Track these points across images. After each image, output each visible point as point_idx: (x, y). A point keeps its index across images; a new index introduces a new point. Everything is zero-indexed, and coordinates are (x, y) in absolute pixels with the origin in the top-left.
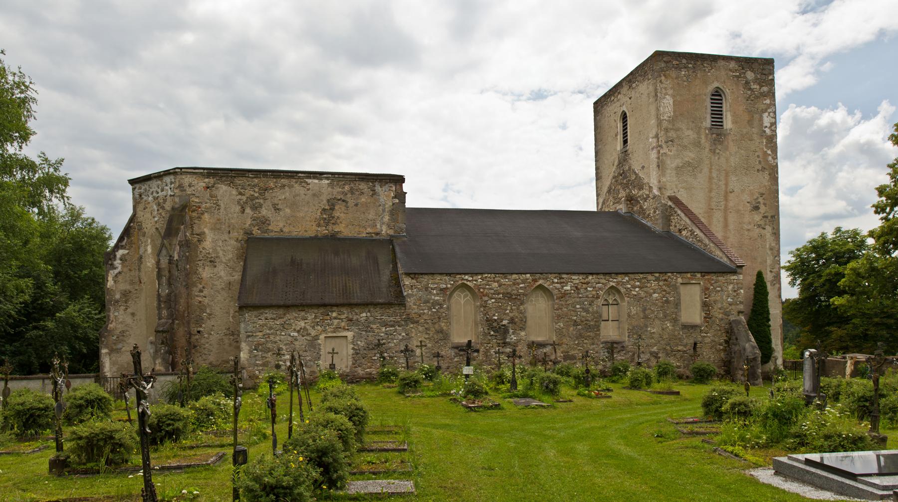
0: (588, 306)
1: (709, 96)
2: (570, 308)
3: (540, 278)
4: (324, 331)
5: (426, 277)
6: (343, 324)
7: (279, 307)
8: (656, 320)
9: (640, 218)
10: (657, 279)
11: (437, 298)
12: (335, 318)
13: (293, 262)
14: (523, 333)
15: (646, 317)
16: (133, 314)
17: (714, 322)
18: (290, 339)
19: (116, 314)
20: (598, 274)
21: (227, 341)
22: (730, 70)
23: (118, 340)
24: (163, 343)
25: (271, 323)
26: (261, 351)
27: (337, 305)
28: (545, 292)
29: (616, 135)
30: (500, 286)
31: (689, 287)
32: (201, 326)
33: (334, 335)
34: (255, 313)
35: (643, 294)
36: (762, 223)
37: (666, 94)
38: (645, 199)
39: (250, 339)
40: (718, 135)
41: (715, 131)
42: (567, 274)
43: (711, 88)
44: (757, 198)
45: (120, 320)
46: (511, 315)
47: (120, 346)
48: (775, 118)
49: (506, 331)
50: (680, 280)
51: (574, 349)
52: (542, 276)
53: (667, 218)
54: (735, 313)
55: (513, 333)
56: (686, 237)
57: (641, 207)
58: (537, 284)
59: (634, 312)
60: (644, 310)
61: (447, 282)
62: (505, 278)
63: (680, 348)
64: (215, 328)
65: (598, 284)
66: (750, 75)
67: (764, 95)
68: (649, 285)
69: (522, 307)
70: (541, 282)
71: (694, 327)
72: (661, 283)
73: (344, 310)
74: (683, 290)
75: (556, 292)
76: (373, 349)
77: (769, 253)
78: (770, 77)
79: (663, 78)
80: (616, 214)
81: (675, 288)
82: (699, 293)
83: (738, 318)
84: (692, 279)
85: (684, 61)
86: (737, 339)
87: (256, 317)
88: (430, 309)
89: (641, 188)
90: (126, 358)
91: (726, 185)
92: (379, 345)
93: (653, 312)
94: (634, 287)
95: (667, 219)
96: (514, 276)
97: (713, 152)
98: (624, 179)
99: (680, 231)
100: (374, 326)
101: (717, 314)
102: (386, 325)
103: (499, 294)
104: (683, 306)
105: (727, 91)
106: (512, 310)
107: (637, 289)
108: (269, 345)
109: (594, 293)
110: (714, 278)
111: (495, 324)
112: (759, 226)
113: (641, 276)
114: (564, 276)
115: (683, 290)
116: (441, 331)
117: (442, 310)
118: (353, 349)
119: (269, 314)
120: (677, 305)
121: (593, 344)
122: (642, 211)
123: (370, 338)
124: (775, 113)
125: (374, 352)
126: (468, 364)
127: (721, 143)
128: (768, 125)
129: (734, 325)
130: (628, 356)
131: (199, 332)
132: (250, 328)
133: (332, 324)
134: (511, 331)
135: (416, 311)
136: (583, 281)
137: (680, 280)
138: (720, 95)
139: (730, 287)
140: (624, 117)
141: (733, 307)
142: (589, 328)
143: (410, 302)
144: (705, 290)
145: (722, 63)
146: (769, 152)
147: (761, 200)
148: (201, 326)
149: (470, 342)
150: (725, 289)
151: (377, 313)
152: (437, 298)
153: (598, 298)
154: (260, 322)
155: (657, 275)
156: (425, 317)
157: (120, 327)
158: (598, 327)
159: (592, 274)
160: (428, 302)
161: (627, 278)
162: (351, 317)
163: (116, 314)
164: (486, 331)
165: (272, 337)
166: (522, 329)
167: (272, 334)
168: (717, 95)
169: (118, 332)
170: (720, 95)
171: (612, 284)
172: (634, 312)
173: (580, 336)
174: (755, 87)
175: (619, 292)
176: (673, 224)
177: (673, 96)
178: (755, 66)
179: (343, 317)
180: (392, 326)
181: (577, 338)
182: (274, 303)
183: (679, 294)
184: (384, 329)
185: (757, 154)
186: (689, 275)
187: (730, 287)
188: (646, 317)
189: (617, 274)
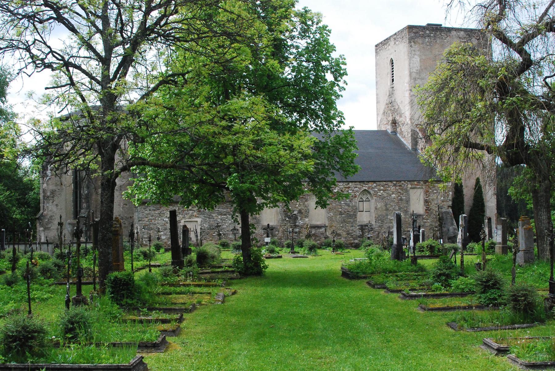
0: (348, 202)
4: (184, 218)
6: (195, 214)
9: (400, 137)
10: (395, 185)
12: (191, 210)
14: (307, 220)
15: (387, 209)
16: (57, 205)
17: (432, 213)
18: (164, 222)
19: (48, 205)
20: (355, 182)
23: (49, 222)
25: (153, 212)
31: (416, 190)
33: (190, 220)
35: (385, 195)
39: (140, 222)
45: (50, 209)
46: (299, 208)
49: (296, 218)
50: (410, 186)
51: (340, 230)
54: (446, 207)
55: (301, 219)
59: (379, 206)
60: (386, 205)
68: (389, 189)
69: (306, 203)
72: (397, 188)
74: (412, 192)
76: (213, 229)
79: (413, 44)
80: (385, 132)
81: (407, 191)
82: (422, 194)
83: (447, 210)
84: (418, 185)
85: (428, 32)
87: (144, 209)
92: (218, 226)
93: (392, 206)
94: (380, 190)
101: (434, 207)
102: (221, 214)
106: (300, 205)
107: (382, 192)
108: (152, 226)
109: (353, 194)
115: (412, 192)
120: (408, 201)
121: (352, 226)
123: (211, 222)
125: (214, 231)
126: (268, 237)
129: (444, 215)
130: (375, 234)
132: (141, 216)
133: (189, 214)
134: (299, 218)
136: (346, 186)
140: (392, 61)
141: (445, 203)
142: (350, 216)
144: (426, 192)
149: (268, 225)
154: (146, 212)
155: (395, 182)
157: (50, 214)
158: (355, 216)
159: (352, 182)
161: (375, 185)
163: (48, 205)
165: (153, 221)
166: (306, 217)
167: (153, 219)
169: (48, 217)
171: (364, 188)
172: (379, 206)
173: (344, 221)
175: (369, 193)
177: (420, 56)
180: (225, 215)
181: (342, 223)
183: (409, 195)
184: (220, 217)
186: (416, 183)
188: (387, 209)
189: (368, 182)
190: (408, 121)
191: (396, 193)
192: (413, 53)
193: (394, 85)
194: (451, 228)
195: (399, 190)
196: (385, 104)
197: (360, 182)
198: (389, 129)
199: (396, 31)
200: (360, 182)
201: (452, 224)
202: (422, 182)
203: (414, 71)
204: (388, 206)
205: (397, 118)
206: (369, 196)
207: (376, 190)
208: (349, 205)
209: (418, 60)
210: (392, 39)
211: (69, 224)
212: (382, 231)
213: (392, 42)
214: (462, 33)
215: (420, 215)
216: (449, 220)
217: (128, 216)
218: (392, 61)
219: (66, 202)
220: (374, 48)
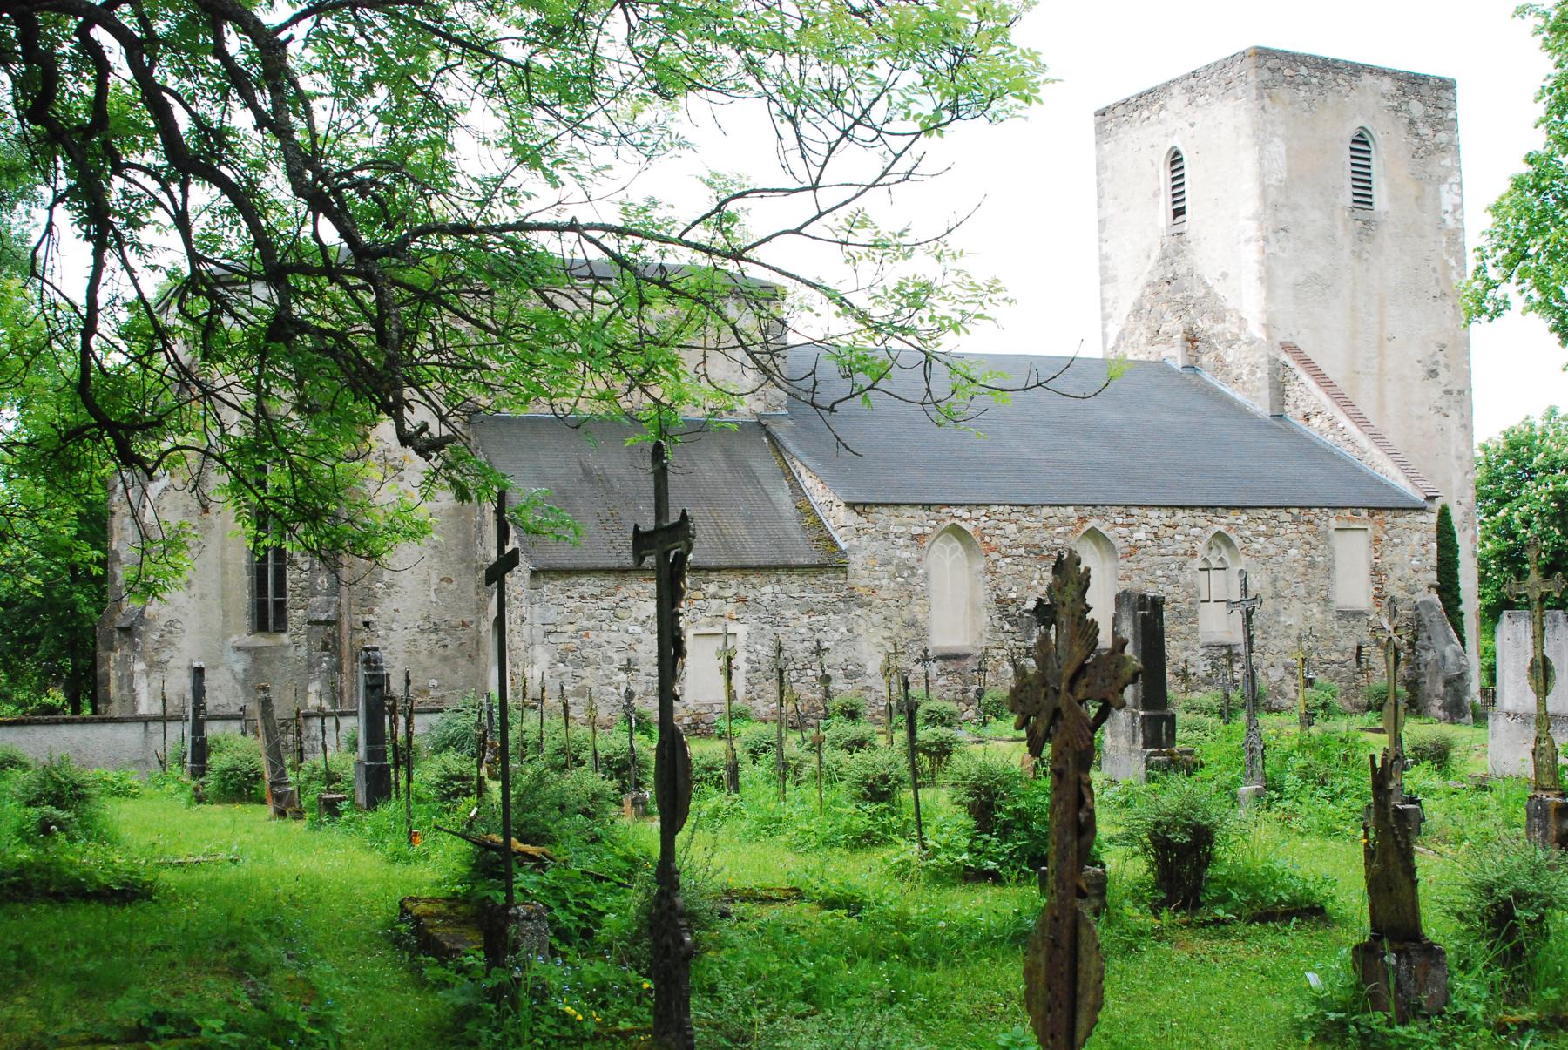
1: (1349, 144)
2: (1145, 576)
3: (1091, 515)
5: (885, 510)
7: (608, 571)
8: (1294, 600)
9: (1215, 382)
10: (1296, 520)
11: (906, 555)
12: (714, 597)
13: (588, 474)
18: (627, 638)
20: (1192, 507)
21: (423, 645)
22: (1383, 96)
24: (325, 647)
25: (591, 605)
26: (572, 663)
27: (718, 569)
28: (1097, 543)
29: (1156, 195)
30: (1020, 531)
32: (371, 612)
34: (560, 584)
35: (1272, 550)
36: (1442, 403)
37: (1273, 134)
38: (1230, 345)
39: (552, 639)
40: (1365, 222)
41: (1360, 214)
42: (1140, 506)
43: (1350, 131)
44: (1434, 354)
47: (164, 656)
48: (1460, 195)
50: (1333, 523)
52: (1095, 511)
53: (1279, 390)
56: (1321, 432)
57: (1219, 359)
58: (1087, 526)
60: (1274, 581)
61: (919, 521)
62: (1030, 514)
63: (1335, 656)
64: (401, 616)
65: (1196, 529)
66: (1417, 108)
67: (1441, 149)
68: (1282, 531)
70: (1093, 523)
71: (1356, 614)
72: (1303, 528)
73: (730, 578)
75: (1119, 543)
77: (1456, 463)
78: (1451, 115)
79: (1267, 101)
80: (1161, 367)
81: (1326, 538)
84: (1354, 520)
85: (1303, 71)
86: (1429, 638)
87: (563, 592)
88: (893, 577)
89: (1219, 317)
90: (179, 684)
91: (1381, 324)
95: (1279, 390)
96: (1047, 511)
97: (1358, 255)
98: (1175, 292)
99: (1306, 417)
100: (788, 614)
103: (1018, 547)
104: (1339, 573)
105: (1378, 136)
108: (587, 652)
110: (1389, 519)
111: (1012, 609)
112: (1438, 410)
113: (1269, 512)
114: (1134, 511)
116: (912, 624)
117: (914, 580)
118: (748, 660)
119: (588, 585)
120: (1329, 571)
121: (1186, 649)
122: (1221, 366)
124: (1460, 185)
127: (1370, 238)
128: (1450, 209)
129: (1423, 611)
131: (366, 624)
135: (866, 581)
136: (1166, 521)
137: (1333, 523)
138: (1366, 143)
139: (1416, 537)
140: (1176, 159)
141: (1420, 576)
143: (856, 562)
145: (1367, 79)
146: (1452, 262)
147: (1440, 357)
148: (371, 612)
150: (1406, 539)
151: (792, 584)
152: (906, 555)
153: (1194, 555)
154: (571, 603)
155: (1295, 511)
156: (883, 594)
159: (1182, 507)
160: (889, 563)
161: (1244, 517)
162: (743, 593)
164: (996, 623)
165: (592, 635)
167: (593, 628)
168: (1361, 143)
170: (1366, 143)
171: (1217, 528)
174: (1425, 130)
175: (1228, 543)
176: (1291, 401)
178: (1425, 90)
179: (728, 593)
180: (821, 613)
182: (602, 563)
183: (1332, 549)
184: (805, 619)
185: (1432, 265)
186: (1348, 513)
187: (1416, 537)
190: (1255, 330)
191: (1298, 543)
192: (1269, 128)
193: (1185, 227)
194: (1448, 651)
195: (1307, 535)
196: (1143, 280)
197: (1205, 508)
198: (1175, 356)
199: (1211, 61)
200: (1205, 508)
201: (1450, 642)
202: (1364, 513)
203: (1273, 182)
204: (1281, 584)
205: (1203, 324)
206: (1225, 553)
207: (1248, 533)
208: (1176, 584)
209: (1283, 150)
210: (1176, 90)
211: (238, 649)
212: (1265, 664)
213: (1178, 100)
214: (1387, 81)
215: (1361, 613)
216: (1439, 628)
217: (456, 621)
218: (1176, 159)
219: (225, 573)
220: (1091, 121)
